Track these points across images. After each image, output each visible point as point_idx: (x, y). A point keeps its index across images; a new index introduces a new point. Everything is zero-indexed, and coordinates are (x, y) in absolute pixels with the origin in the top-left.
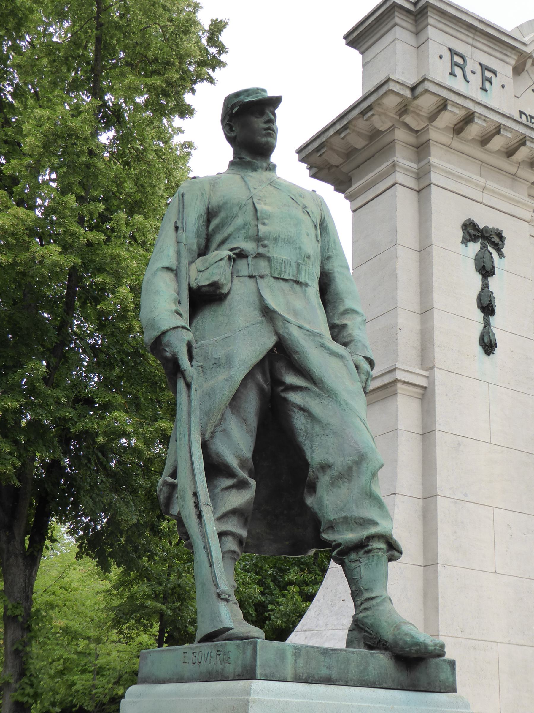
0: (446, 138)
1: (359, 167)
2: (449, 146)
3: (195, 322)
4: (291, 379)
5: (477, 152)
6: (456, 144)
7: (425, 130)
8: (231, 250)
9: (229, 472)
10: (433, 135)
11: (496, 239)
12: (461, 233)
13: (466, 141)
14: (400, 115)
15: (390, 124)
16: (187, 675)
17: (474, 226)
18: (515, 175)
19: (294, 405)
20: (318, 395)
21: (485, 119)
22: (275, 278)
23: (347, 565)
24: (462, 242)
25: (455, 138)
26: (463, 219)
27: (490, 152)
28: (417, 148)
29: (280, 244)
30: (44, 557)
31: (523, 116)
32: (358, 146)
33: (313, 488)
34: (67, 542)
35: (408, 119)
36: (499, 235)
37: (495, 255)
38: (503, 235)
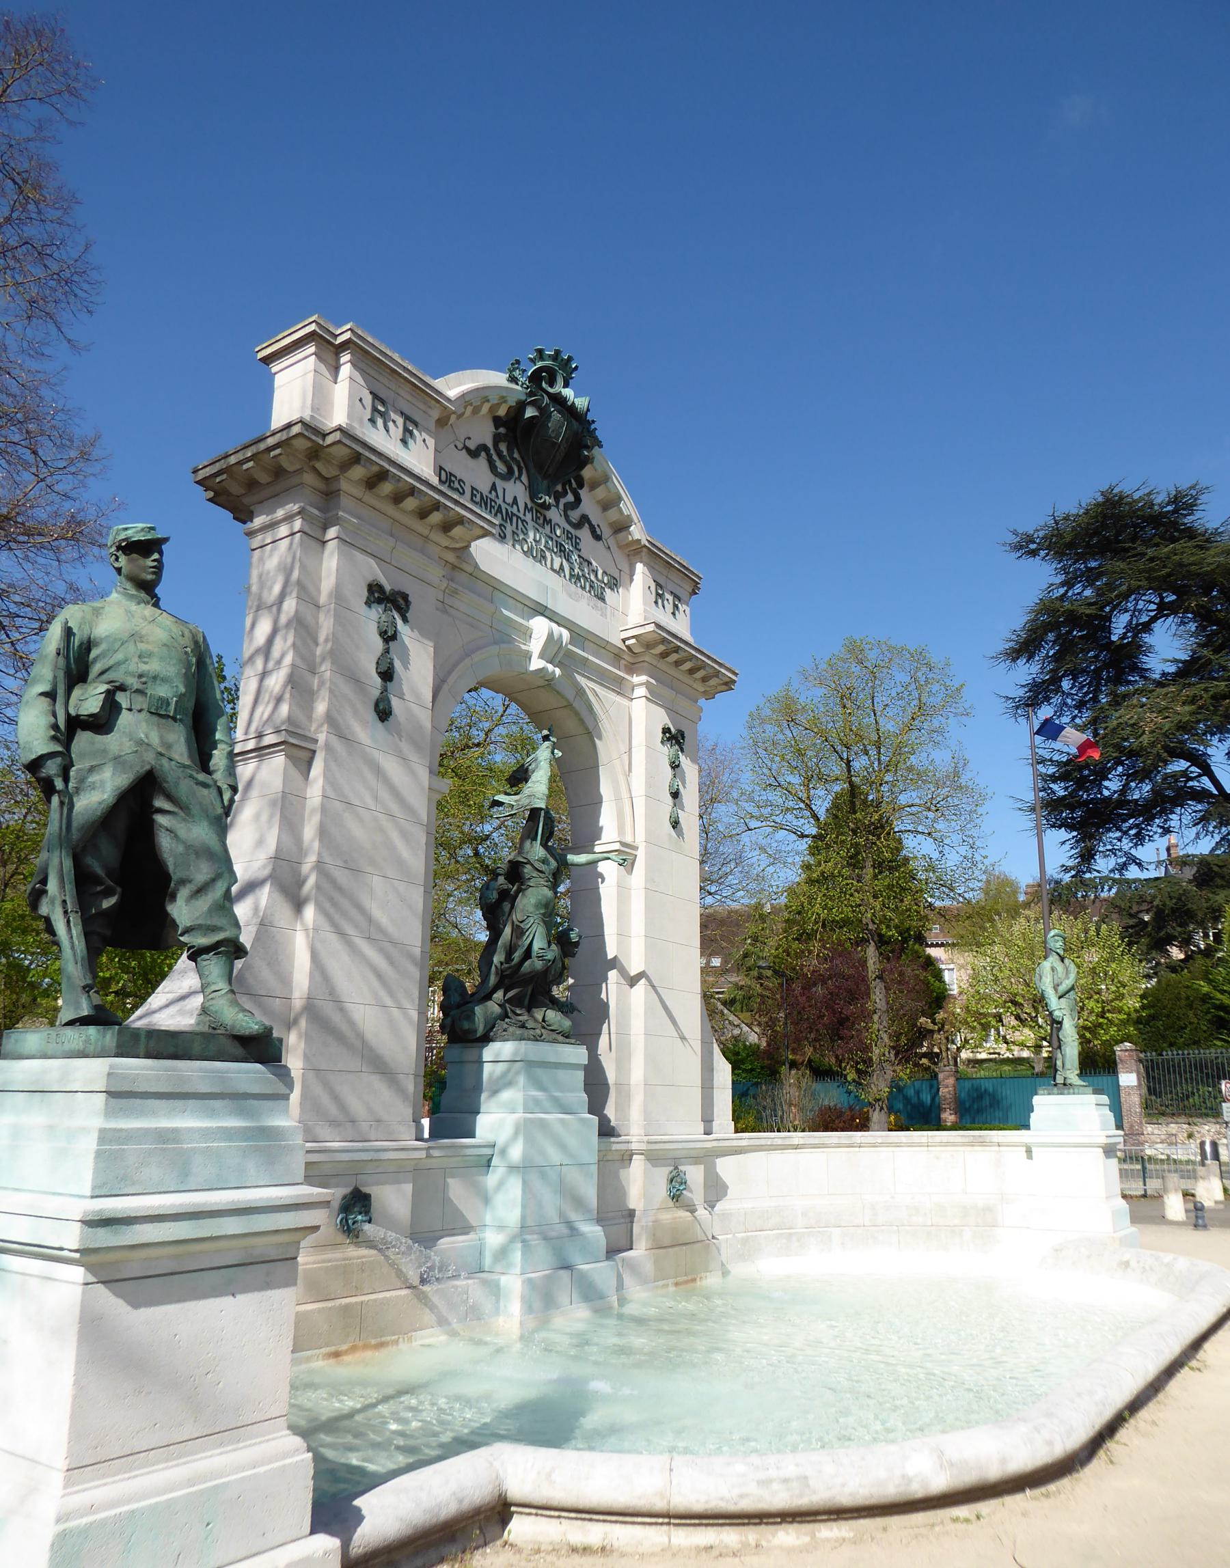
0: (358, 491)
1: (262, 502)
2: (360, 500)
3: (43, 698)
4: (160, 803)
5: (390, 509)
6: (368, 498)
7: (336, 478)
8: (107, 683)
9: (97, 880)
10: (344, 485)
11: (401, 601)
12: (366, 594)
13: (378, 496)
14: (310, 459)
15: (298, 466)
16: (49, 1053)
17: (380, 588)
18: (426, 538)
19: (161, 826)
20: (184, 820)
21: (399, 479)
22: (151, 713)
23: (1195, 908)
24: (366, 603)
25: (367, 492)
26: (370, 579)
27: (403, 511)
28: (327, 495)
29: (158, 682)
30: (1167, 831)
31: (443, 472)
32: (263, 481)
33: (173, 898)
34: (1106, 887)
35: (319, 465)
36: (405, 597)
37: (399, 622)
38: (410, 599)
